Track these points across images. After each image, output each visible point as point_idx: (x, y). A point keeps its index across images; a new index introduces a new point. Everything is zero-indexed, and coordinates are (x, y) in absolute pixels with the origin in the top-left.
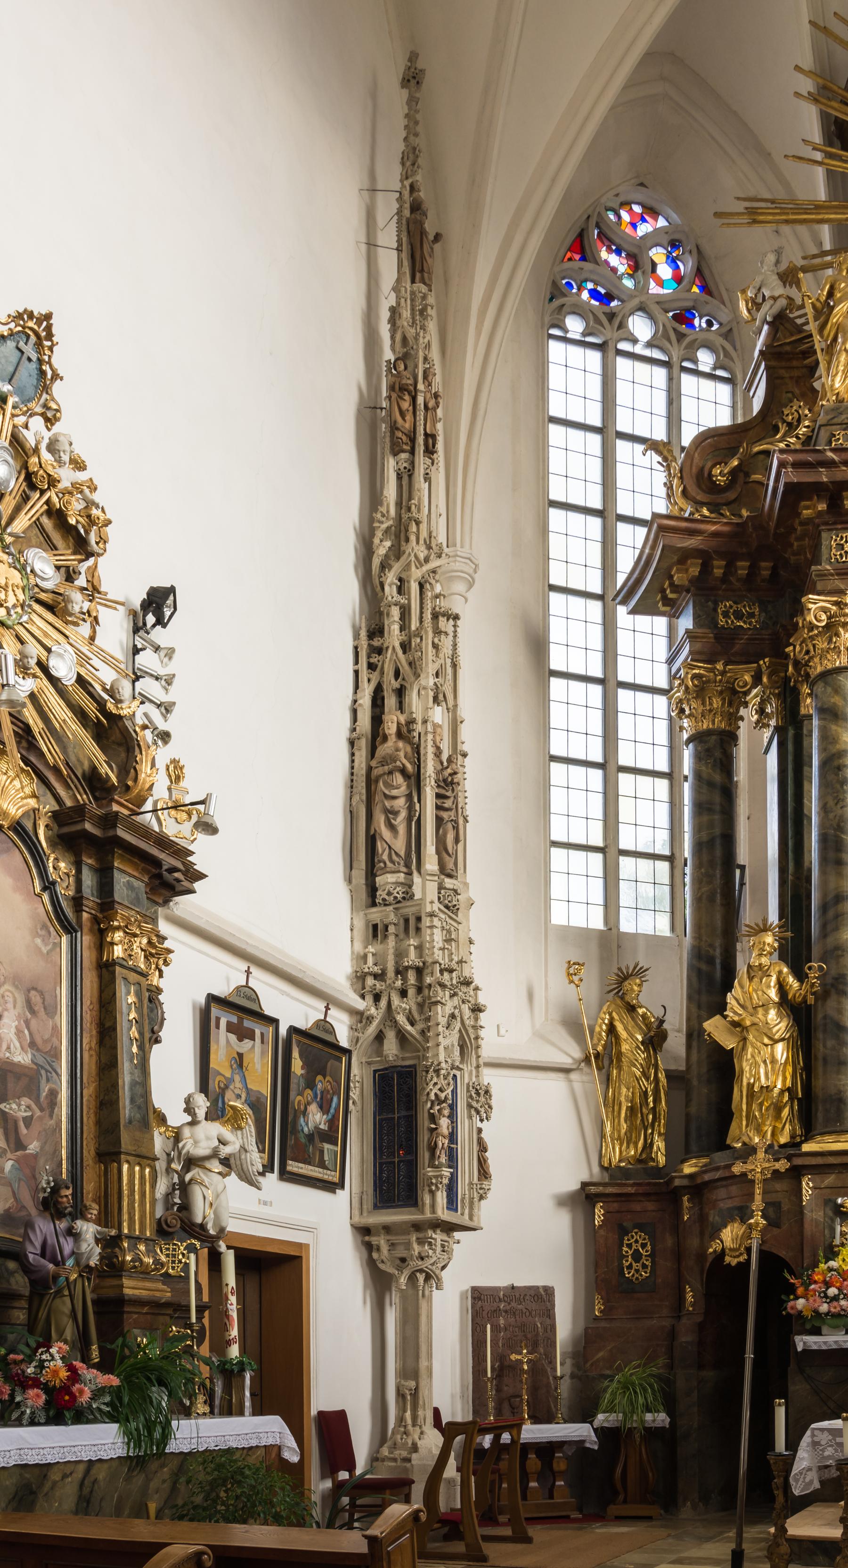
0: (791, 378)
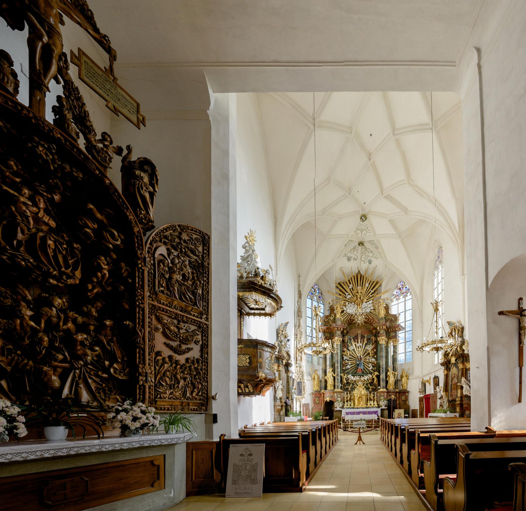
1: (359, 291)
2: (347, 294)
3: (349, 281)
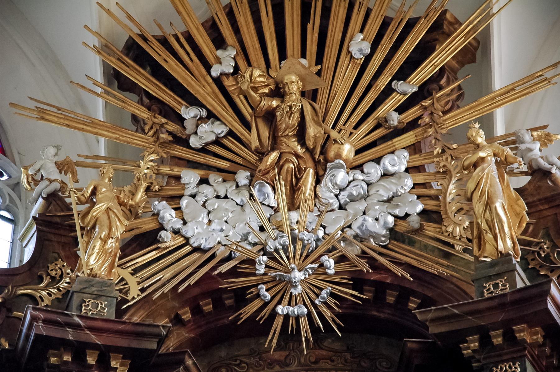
0: (59, 243)
1: (294, 84)
2: (189, 113)
3: (212, 28)
